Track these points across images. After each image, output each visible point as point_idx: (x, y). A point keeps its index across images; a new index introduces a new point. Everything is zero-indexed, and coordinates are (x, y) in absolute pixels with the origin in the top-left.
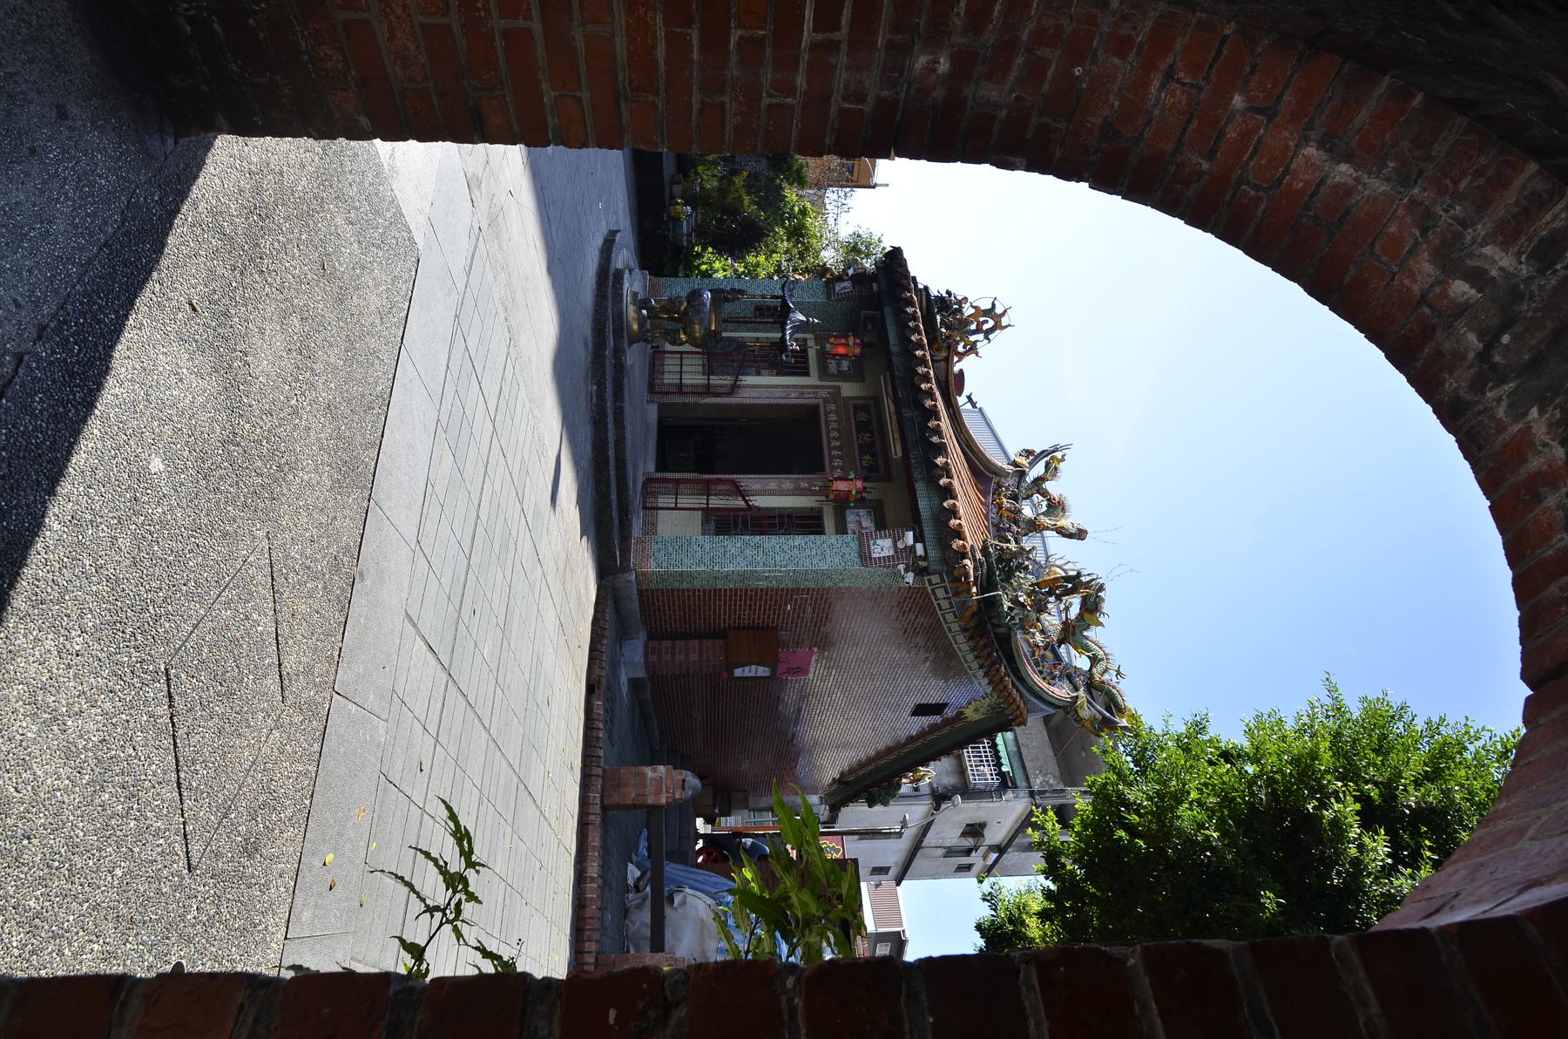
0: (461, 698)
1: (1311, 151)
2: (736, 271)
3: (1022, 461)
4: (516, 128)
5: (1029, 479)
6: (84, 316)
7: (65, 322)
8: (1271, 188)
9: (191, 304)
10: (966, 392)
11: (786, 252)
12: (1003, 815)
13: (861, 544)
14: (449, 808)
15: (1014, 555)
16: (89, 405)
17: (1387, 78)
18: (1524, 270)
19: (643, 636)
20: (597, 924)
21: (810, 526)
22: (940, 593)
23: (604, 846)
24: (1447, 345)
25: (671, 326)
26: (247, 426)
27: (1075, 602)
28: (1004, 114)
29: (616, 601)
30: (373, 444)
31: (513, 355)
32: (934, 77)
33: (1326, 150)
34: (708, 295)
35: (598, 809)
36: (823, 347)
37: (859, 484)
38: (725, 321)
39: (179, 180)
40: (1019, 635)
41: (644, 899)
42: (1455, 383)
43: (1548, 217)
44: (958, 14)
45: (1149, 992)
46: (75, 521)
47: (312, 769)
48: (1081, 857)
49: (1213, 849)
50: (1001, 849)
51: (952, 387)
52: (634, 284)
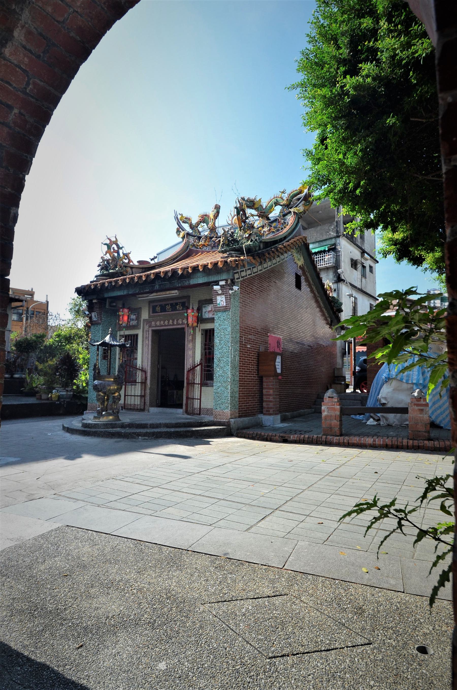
0: (288, 504)
2: (87, 369)
3: (182, 234)
5: (190, 231)
8: (28, 76)
9: (79, 648)
10: (149, 261)
11: (78, 345)
13: (219, 311)
15: (226, 238)
19: (261, 416)
20: (395, 439)
21: (210, 336)
22: (243, 274)
23: (359, 435)
25: (111, 399)
26: (146, 616)
27: (249, 211)
31: (121, 477)
33: (7, 43)
34: (96, 382)
35: (342, 438)
36: (124, 327)
37: (189, 311)
38: (109, 374)
39: (11, 656)
40: (264, 238)
47: (321, 579)
48: (368, 212)
49: (366, 148)
50: (363, 252)
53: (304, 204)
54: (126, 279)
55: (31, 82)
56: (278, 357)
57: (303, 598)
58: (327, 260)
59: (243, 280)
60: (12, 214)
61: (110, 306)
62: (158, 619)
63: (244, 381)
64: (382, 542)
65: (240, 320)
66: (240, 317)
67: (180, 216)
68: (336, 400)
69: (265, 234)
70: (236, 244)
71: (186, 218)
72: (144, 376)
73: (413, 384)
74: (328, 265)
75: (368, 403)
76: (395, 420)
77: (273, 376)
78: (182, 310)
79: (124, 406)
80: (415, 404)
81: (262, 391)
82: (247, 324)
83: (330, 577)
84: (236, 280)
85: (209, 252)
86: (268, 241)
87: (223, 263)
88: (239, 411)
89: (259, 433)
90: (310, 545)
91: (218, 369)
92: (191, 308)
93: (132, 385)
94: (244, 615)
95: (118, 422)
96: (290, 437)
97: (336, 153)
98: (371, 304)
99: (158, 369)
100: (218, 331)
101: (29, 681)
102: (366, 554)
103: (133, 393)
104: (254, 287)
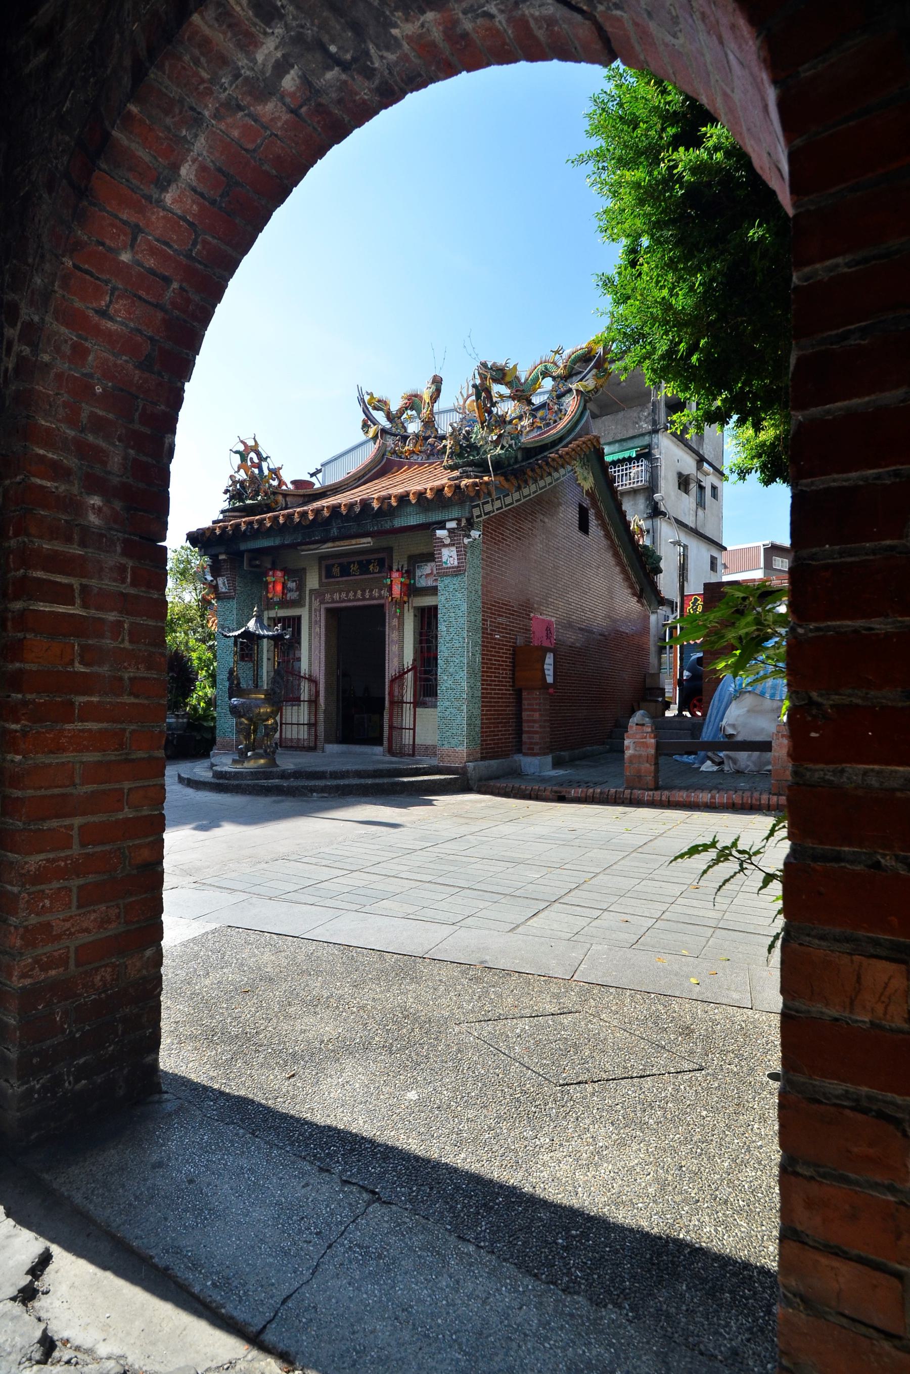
1: (168, 198)
3: (372, 431)
4: (151, 839)
6: (307, 1145)
7: (315, 1156)
8: (195, 231)
9: (289, 1078)
10: (307, 478)
12: (672, 456)
13: (446, 575)
14: (676, 858)
15: (457, 442)
16: (371, 1142)
17: (114, 133)
18: (279, 31)
19: (518, 757)
20: (747, 794)
22: (488, 508)
23: (687, 788)
26: (377, 1039)
27: (498, 389)
28: (132, 452)
29: (490, 778)
32: (105, 509)
33: (169, 185)
34: (234, 701)
37: (395, 575)
39: (195, 1089)
40: (523, 439)
41: (729, 757)
42: (364, 90)
43: (238, 9)
44: (57, 488)
46: (459, 1144)
47: (628, 993)
48: (713, 394)
49: (713, 280)
50: (701, 460)
51: (308, 491)
52: (225, 763)
53: (596, 375)
54: (278, 517)
55: (199, 240)
56: (548, 655)
57: (603, 1016)
58: (633, 477)
59: (488, 519)
60: (166, 445)
62: (396, 1043)
63: (491, 698)
64: (720, 887)
65: (483, 590)
66: (482, 585)
67: (369, 397)
68: (649, 730)
69: (525, 432)
70: (475, 453)
71: (379, 401)
72: (313, 689)
74: (635, 485)
75: (703, 734)
76: (748, 763)
77: (540, 689)
78: (379, 572)
81: (521, 714)
82: (494, 597)
83: (643, 989)
84: (476, 520)
85: (423, 464)
87: (453, 489)
88: (482, 749)
89: (517, 785)
90: (610, 950)
91: (446, 678)
93: (292, 705)
94: (519, 1036)
95: (275, 769)
97: (657, 285)
99: (338, 677)
100: (445, 611)
101: (230, 1117)
102: (696, 961)
103: (297, 719)
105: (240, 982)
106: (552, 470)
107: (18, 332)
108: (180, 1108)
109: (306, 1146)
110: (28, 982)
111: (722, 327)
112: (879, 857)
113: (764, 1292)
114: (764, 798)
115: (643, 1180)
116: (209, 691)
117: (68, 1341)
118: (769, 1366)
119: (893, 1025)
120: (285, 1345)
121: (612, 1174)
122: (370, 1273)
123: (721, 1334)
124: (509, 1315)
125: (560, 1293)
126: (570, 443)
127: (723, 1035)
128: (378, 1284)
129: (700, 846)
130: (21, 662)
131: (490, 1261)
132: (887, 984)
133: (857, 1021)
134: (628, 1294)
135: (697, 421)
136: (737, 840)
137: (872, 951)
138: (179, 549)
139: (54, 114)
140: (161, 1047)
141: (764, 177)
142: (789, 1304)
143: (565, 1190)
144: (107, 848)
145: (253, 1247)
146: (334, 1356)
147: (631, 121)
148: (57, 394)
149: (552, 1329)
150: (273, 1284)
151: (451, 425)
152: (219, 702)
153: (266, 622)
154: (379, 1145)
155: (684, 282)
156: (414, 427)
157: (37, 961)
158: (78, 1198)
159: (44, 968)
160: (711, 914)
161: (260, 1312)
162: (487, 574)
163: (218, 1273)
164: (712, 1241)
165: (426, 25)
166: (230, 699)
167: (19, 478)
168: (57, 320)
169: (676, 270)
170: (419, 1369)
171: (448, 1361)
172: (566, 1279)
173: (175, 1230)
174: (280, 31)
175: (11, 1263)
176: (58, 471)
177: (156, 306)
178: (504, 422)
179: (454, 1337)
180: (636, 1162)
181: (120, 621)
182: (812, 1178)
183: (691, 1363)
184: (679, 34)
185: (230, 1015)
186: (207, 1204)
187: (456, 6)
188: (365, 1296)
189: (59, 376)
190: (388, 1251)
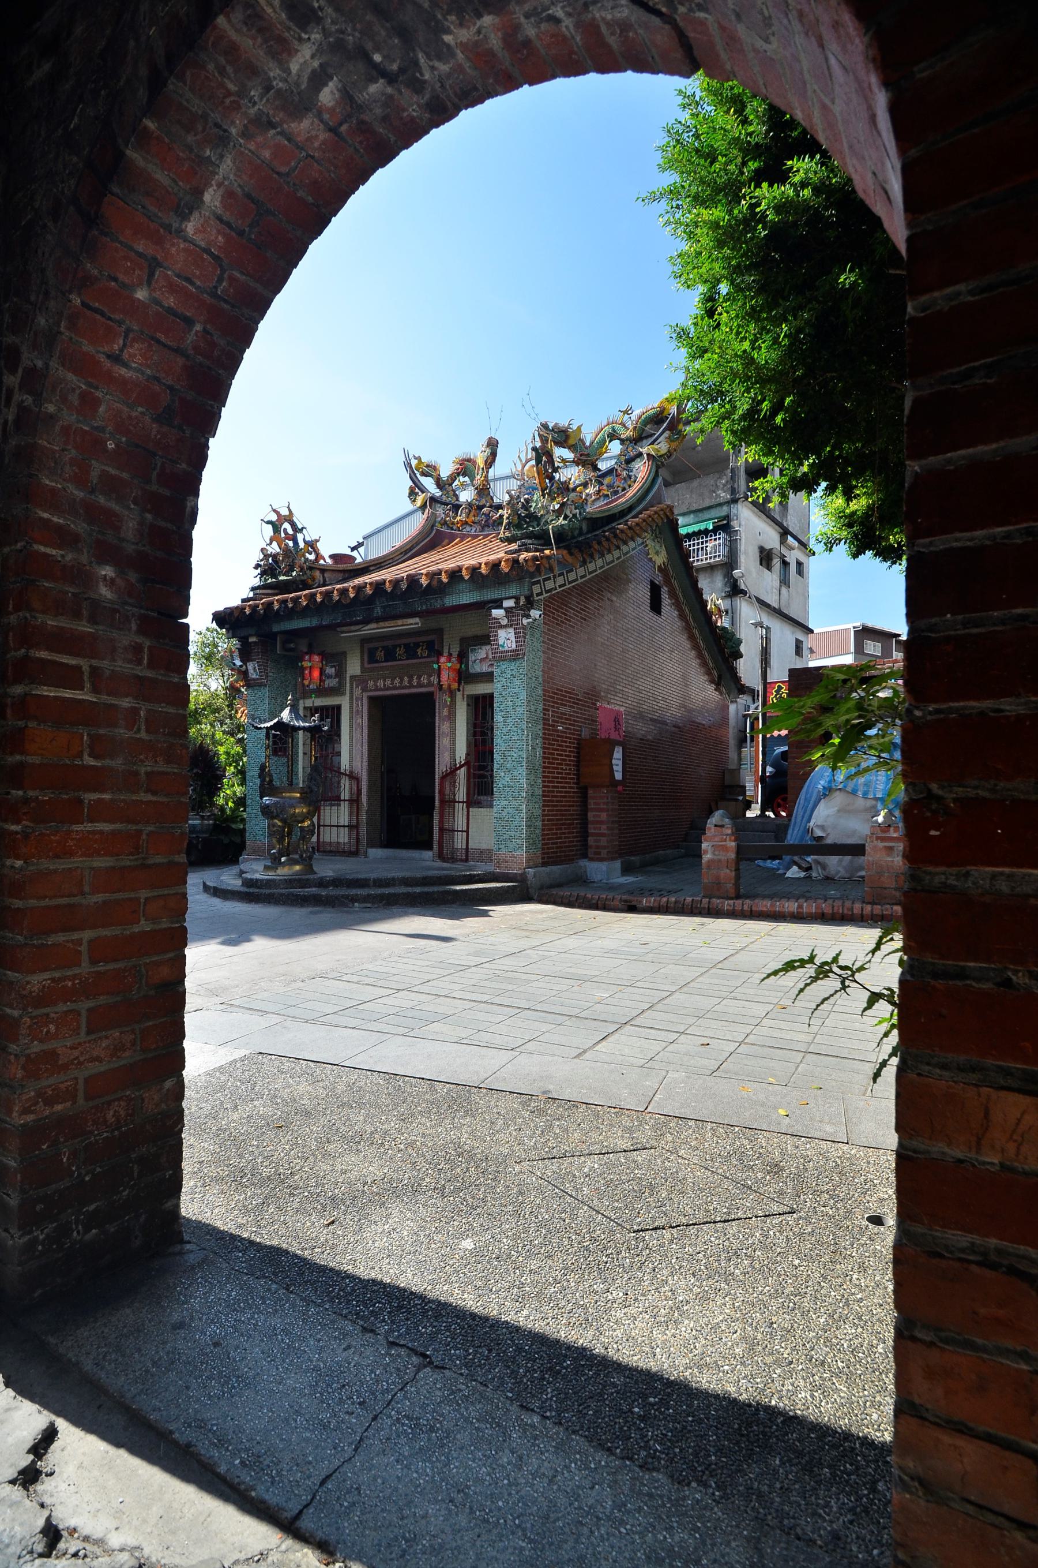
0: (645, 1015)
3: (420, 499)
4: (171, 955)
5: (436, 491)
6: (349, 1302)
7: (357, 1314)
8: (221, 266)
9: (328, 1225)
10: (348, 552)
12: (753, 529)
13: (503, 659)
14: (769, 976)
15: (515, 512)
16: (422, 1297)
17: (128, 152)
18: (316, 36)
19: (584, 863)
21: (484, 708)
22: (550, 585)
23: (771, 897)
24: (378, 111)
27: (561, 453)
28: (149, 516)
30: (431, 1087)
31: (335, 975)
33: (191, 213)
36: (312, 691)
37: (443, 660)
39: (222, 1239)
41: (817, 862)
42: (413, 106)
43: (269, 10)
44: (63, 556)
45: (940, 457)
46: (521, 1299)
49: (799, 331)
50: (785, 533)
51: (349, 566)
52: (256, 869)
53: (669, 438)
54: (315, 594)
55: (226, 276)
57: (681, 1152)
58: (710, 551)
59: (550, 597)
60: (188, 509)
61: (284, 648)
62: (449, 1184)
65: (543, 676)
66: (543, 671)
67: (416, 461)
68: (729, 831)
70: (535, 524)
71: (428, 466)
72: (355, 787)
73: (876, 799)
74: (712, 560)
75: (789, 837)
76: (840, 869)
77: (608, 786)
79: (318, 846)
80: (878, 838)
81: (586, 815)
83: (726, 1122)
84: (536, 598)
85: (477, 536)
86: (598, 516)
87: (510, 564)
88: (543, 853)
89: (582, 894)
90: (688, 1077)
92: (446, 654)
93: (331, 805)
95: (311, 877)
96: (641, 902)
98: (797, 640)
100: (501, 699)
102: (785, 1090)
104: (569, 609)
105: (272, 1116)
106: (621, 543)
107: (18, 381)
108: (204, 1261)
109: (347, 1303)
110: (30, 1118)
111: (809, 384)
112: (1010, 974)
113: (868, 1466)
114: (857, 907)
115: (729, 1339)
116: (238, 790)
117: (75, 1530)
118: (875, 1552)
119: (1026, 1167)
120: (324, 1533)
121: (694, 1333)
122: (420, 1449)
123: (820, 1516)
124: (579, 1496)
125: (637, 1469)
126: (640, 513)
127: (816, 1173)
128: (430, 1461)
129: (795, 961)
130: (22, 754)
131: (557, 1433)
132: (1019, 1120)
133: (984, 1163)
134: (714, 1470)
135: (781, 488)
136: (838, 955)
137: (1002, 1082)
138: (204, 631)
139: (60, 131)
140: (183, 1190)
141: (867, 202)
142: (905, 1487)
143: (641, 1351)
144: (120, 965)
145: (287, 1420)
146: (379, 1545)
147: (708, 154)
148: (63, 450)
149: (629, 1512)
150: (310, 1463)
151: (508, 492)
152: (249, 802)
153: (301, 713)
154: (431, 1301)
155: (767, 333)
156: (466, 496)
157: (40, 1094)
158: (88, 1365)
159: (49, 1102)
160: (802, 1037)
161: (295, 1495)
162: (548, 658)
163: (247, 1450)
164: (808, 1408)
165: (484, 31)
166: (261, 798)
167: (19, 546)
168: (63, 365)
169: (758, 320)
170: (478, 1559)
171: (510, 1550)
172: (643, 1453)
173: (198, 1400)
174: (318, 36)
175: (10, 1440)
176: (64, 538)
177: (177, 351)
178: (568, 489)
179: (517, 1522)
180: (721, 1318)
181: (135, 708)
182: (932, 1344)
183: (786, 1549)
184: (772, 38)
185: (261, 1154)
186: (234, 1370)
187: (517, 8)
188: (415, 1475)
189: (66, 430)
190: (441, 1423)
